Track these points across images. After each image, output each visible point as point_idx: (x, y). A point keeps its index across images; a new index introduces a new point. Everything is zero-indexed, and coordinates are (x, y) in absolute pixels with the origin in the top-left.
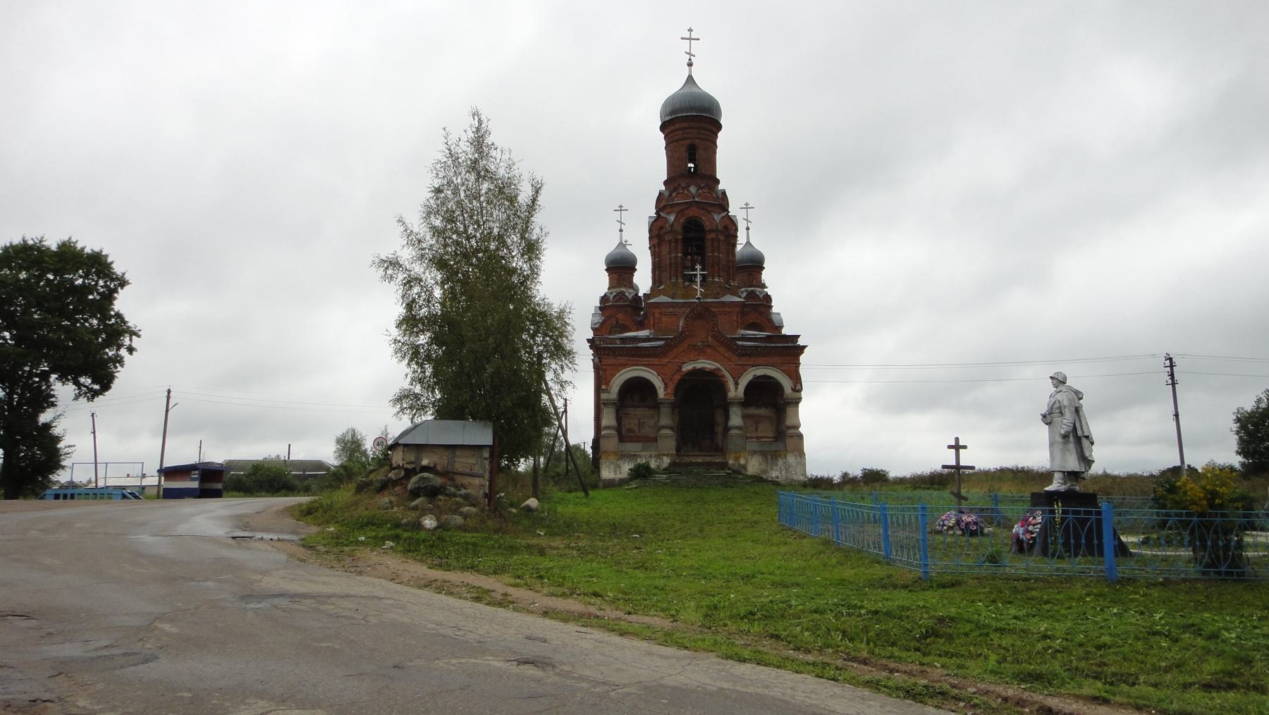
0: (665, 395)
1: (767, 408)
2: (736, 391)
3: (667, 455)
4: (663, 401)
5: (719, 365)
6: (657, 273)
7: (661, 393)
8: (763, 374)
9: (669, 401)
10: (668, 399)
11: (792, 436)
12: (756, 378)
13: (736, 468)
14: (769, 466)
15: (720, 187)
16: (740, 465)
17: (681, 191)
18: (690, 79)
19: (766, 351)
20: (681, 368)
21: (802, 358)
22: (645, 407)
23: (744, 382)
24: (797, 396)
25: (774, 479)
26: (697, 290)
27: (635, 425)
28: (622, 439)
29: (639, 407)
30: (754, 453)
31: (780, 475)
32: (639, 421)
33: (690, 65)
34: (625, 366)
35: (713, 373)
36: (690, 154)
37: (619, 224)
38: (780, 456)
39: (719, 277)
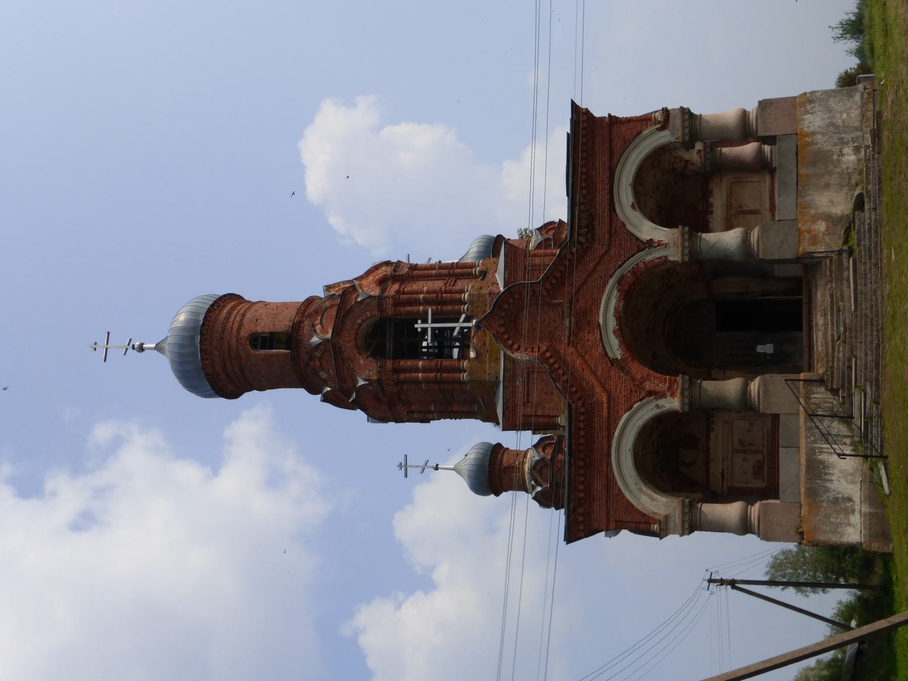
0: (673, 395)
1: (711, 193)
4: (687, 401)
5: (611, 281)
6: (455, 408)
7: (673, 403)
9: (687, 386)
12: (640, 204)
15: (321, 294)
17: (318, 363)
18: (159, 348)
20: (614, 362)
21: (599, 111)
22: (708, 439)
23: (647, 230)
24: (679, 116)
26: (462, 328)
27: (745, 460)
28: (771, 491)
29: (708, 449)
32: (738, 451)
33: (141, 349)
34: (610, 481)
37: (422, 464)
39: (462, 291)
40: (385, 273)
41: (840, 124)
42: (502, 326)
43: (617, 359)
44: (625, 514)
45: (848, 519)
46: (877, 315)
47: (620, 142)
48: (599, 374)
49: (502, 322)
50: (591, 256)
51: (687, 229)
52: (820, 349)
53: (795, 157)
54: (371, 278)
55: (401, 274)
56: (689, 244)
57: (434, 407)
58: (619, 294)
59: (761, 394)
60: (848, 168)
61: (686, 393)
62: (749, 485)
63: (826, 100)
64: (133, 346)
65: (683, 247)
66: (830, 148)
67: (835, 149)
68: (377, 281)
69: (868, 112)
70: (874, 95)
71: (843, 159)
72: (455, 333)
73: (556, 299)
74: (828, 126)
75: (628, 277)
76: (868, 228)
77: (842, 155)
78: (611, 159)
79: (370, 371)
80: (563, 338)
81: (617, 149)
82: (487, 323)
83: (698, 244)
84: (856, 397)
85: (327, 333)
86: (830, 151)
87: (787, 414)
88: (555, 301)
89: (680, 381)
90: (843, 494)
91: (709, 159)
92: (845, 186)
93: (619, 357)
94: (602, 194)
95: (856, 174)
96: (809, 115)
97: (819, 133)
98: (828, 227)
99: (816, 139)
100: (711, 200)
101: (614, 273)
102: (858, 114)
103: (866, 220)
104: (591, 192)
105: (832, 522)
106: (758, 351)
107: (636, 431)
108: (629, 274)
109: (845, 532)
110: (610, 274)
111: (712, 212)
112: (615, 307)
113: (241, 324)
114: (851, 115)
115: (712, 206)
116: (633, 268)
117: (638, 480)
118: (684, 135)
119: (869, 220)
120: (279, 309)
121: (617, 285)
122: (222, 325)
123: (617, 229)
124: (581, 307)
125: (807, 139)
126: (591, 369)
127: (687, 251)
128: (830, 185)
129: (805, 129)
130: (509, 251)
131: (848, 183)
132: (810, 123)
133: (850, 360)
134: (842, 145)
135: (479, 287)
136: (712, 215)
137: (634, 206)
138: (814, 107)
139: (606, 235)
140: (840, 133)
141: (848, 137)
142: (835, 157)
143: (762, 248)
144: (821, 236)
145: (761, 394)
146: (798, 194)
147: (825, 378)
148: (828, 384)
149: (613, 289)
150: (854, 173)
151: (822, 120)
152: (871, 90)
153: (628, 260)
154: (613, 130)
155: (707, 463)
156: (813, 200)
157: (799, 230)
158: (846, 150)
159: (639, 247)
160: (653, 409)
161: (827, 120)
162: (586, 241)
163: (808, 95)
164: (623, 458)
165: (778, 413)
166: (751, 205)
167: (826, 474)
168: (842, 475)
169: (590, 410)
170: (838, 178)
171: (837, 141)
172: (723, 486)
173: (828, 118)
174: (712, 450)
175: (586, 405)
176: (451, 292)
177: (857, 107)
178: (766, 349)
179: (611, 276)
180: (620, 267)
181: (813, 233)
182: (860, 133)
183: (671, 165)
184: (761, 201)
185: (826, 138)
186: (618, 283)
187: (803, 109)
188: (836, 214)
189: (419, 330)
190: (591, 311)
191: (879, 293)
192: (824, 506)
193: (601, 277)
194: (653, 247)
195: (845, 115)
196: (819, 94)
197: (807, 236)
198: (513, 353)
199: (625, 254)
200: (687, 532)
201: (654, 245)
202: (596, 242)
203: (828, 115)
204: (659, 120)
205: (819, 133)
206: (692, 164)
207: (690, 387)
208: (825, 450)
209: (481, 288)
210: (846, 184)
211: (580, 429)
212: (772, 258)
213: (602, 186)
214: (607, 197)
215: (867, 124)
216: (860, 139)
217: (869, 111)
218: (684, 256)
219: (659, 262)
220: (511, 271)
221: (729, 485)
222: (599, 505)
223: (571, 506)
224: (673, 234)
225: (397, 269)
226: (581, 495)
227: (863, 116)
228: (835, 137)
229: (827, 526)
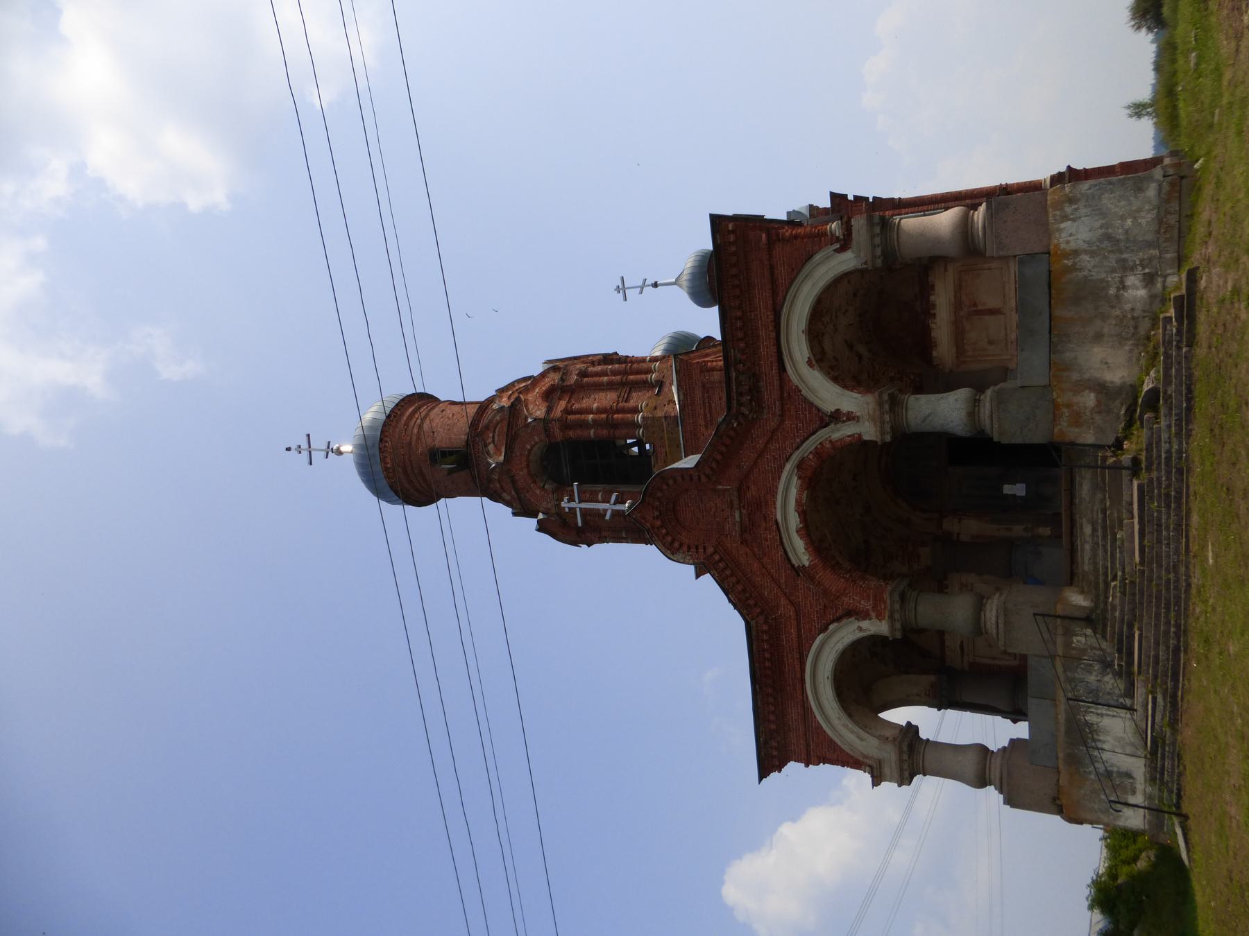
0: (880, 617)
1: (933, 287)
4: (898, 625)
5: (788, 467)
7: (878, 627)
8: (803, 337)
9: (897, 606)
12: (819, 359)
16: (1100, 408)
19: (740, 334)
20: (797, 571)
35: (812, 480)
37: (640, 283)
39: (636, 411)
40: (552, 382)
41: (1121, 237)
42: (657, 518)
43: (804, 565)
44: (828, 750)
46: (1177, 602)
47: (784, 269)
48: (782, 581)
49: (657, 513)
50: (759, 430)
52: (1086, 568)
53: (1046, 289)
54: (537, 390)
55: (568, 384)
56: (890, 416)
57: (626, 534)
58: (799, 482)
59: (1001, 626)
60: (1133, 310)
61: (897, 616)
63: (1096, 197)
64: (332, 449)
65: (883, 422)
66: (1103, 276)
67: (1112, 278)
68: (543, 393)
69: (1169, 216)
70: (1180, 186)
71: (1125, 294)
72: (607, 517)
73: (720, 484)
74: (1100, 240)
76: (1166, 458)
77: (1124, 288)
78: (774, 293)
79: (547, 502)
80: (734, 534)
81: (782, 280)
82: (639, 514)
83: (904, 416)
84: (1139, 689)
85: (500, 455)
86: (1102, 280)
88: (720, 487)
90: (1118, 768)
92: (1128, 339)
93: (807, 564)
94: (767, 345)
95: (1147, 319)
96: (1069, 223)
97: (1085, 252)
98: (1099, 403)
99: (1080, 262)
100: (932, 298)
101: (791, 454)
102: (1153, 219)
103: (1163, 444)
104: (751, 342)
106: (1004, 492)
108: (811, 456)
110: (786, 456)
112: (796, 499)
113: (419, 438)
114: (1139, 221)
115: (934, 306)
116: (816, 448)
117: (841, 713)
118: (874, 257)
119: (1168, 445)
120: (455, 417)
121: (796, 471)
122: (383, 460)
123: (790, 395)
124: (752, 496)
125: (1066, 261)
126: (772, 577)
127: (888, 428)
128: (1103, 335)
129: (1063, 246)
130: (680, 366)
131: (1134, 334)
132: (1071, 235)
133: (1131, 626)
134: (1124, 272)
135: (653, 406)
136: (935, 318)
137: (811, 363)
138: (1076, 209)
139: (777, 403)
140: (1121, 252)
141: (1132, 258)
142: (1112, 291)
143: (997, 426)
144: (1088, 413)
145: (1001, 626)
146: (1052, 348)
147: (1094, 616)
148: (1098, 626)
149: (791, 475)
150: (1144, 317)
151: (1090, 231)
152: (1175, 177)
153: (807, 438)
154: (774, 252)
156: (1076, 358)
157: (1053, 401)
158: (1131, 280)
159: (822, 419)
160: (854, 631)
161: (1100, 230)
162: (750, 412)
164: (821, 687)
165: (1026, 653)
166: (991, 302)
167: (1094, 740)
168: (1117, 744)
169: (776, 625)
170: (1116, 325)
171: (1116, 265)
172: (962, 661)
173: (1101, 227)
175: (770, 621)
176: (623, 411)
177: (1151, 207)
178: (1017, 489)
179: (787, 460)
180: (798, 448)
181: (1075, 408)
182: (1155, 252)
184: (1004, 297)
185: (1097, 259)
186: (797, 468)
187: (1058, 213)
188: (1112, 382)
189: (567, 510)
190: (767, 502)
191: (1182, 569)
192: (1091, 779)
193: (775, 459)
194: (840, 421)
195: (1129, 222)
197: (1066, 411)
198: (673, 554)
201: (842, 419)
202: (765, 410)
203: (1101, 222)
204: (837, 235)
205: (1085, 252)
207: (901, 608)
208: (1093, 710)
209: (655, 408)
210: (1129, 336)
211: (764, 650)
212: (1013, 441)
213: (765, 333)
214: (774, 349)
215: (1168, 236)
216: (1155, 262)
217: (1171, 214)
218: (884, 434)
219: (850, 440)
220: (686, 391)
222: (797, 736)
223: (762, 739)
224: (868, 403)
225: (564, 377)
226: (773, 727)
227: (1160, 222)
228: (1113, 258)
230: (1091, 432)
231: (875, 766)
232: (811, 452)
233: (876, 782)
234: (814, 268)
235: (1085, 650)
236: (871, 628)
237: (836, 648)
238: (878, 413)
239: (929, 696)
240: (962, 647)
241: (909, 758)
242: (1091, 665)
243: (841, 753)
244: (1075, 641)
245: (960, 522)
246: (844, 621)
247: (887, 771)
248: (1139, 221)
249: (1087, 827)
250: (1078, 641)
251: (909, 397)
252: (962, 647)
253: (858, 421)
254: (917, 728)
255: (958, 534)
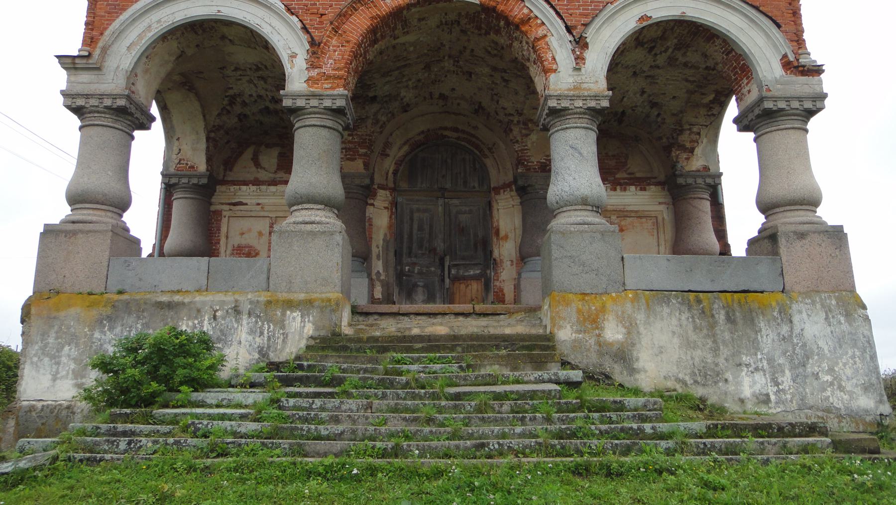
2: (577, 69)
3: (306, 306)
9: (328, 103)
10: (320, 97)
11: (802, 236)
13: (591, 359)
14: (725, 352)
25: (750, 406)
27: (260, 234)
30: (661, 295)
31: (771, 390)
36: (254, 155)
38: (764, 309)
41: (809, 370)
45: (66, 377)
51: (605, 104)
61: (314, 102)
62: (223, 241)
65: (572, 98)
69: (836, 420)
75: (520, 11)
87: (269, 270)
89: (335, 92)
91: (695, 182)
100: (633, 188)
105: (63, 348)
107: (252, 22)
108: (525, 11)
109: (42, 371)
111: (615, 190)
116: (537, 17)
136: (611, 190)
142: (745, 359)
155: (257, 182)
163: (861, 311)
172: (222, 204)
174: (273, 189)
183: (688, 127)
196: (865, 332)
199: (562, 5)
200: (70, 103)
206: (688, 159)
221: (224, 213)
229: (57, 338)
230: (574, 335)
231: (90, 61)
232: (532, 11)
233: (68, 62)
234: (764, 31)
235: (283, 327)
236: (295, 69)
237: (264, 25)
238: (586, 94)
239: (179, 163)
240: (241, 204)
241: (106, 107)
242: (262, 333)
243: (107, 20)
244: (295, 314)
245: (386, 208)
246: (305, 37)
247: (85, 77)
248: (829, 389)
249: (19, 327)
250: (294, 318)
251: (595, 132)
252: (241, 204)
253: (575, 69)
254: (148, 128)
255: (373, 205)
